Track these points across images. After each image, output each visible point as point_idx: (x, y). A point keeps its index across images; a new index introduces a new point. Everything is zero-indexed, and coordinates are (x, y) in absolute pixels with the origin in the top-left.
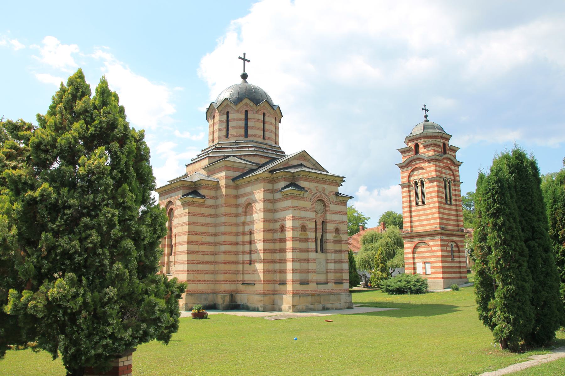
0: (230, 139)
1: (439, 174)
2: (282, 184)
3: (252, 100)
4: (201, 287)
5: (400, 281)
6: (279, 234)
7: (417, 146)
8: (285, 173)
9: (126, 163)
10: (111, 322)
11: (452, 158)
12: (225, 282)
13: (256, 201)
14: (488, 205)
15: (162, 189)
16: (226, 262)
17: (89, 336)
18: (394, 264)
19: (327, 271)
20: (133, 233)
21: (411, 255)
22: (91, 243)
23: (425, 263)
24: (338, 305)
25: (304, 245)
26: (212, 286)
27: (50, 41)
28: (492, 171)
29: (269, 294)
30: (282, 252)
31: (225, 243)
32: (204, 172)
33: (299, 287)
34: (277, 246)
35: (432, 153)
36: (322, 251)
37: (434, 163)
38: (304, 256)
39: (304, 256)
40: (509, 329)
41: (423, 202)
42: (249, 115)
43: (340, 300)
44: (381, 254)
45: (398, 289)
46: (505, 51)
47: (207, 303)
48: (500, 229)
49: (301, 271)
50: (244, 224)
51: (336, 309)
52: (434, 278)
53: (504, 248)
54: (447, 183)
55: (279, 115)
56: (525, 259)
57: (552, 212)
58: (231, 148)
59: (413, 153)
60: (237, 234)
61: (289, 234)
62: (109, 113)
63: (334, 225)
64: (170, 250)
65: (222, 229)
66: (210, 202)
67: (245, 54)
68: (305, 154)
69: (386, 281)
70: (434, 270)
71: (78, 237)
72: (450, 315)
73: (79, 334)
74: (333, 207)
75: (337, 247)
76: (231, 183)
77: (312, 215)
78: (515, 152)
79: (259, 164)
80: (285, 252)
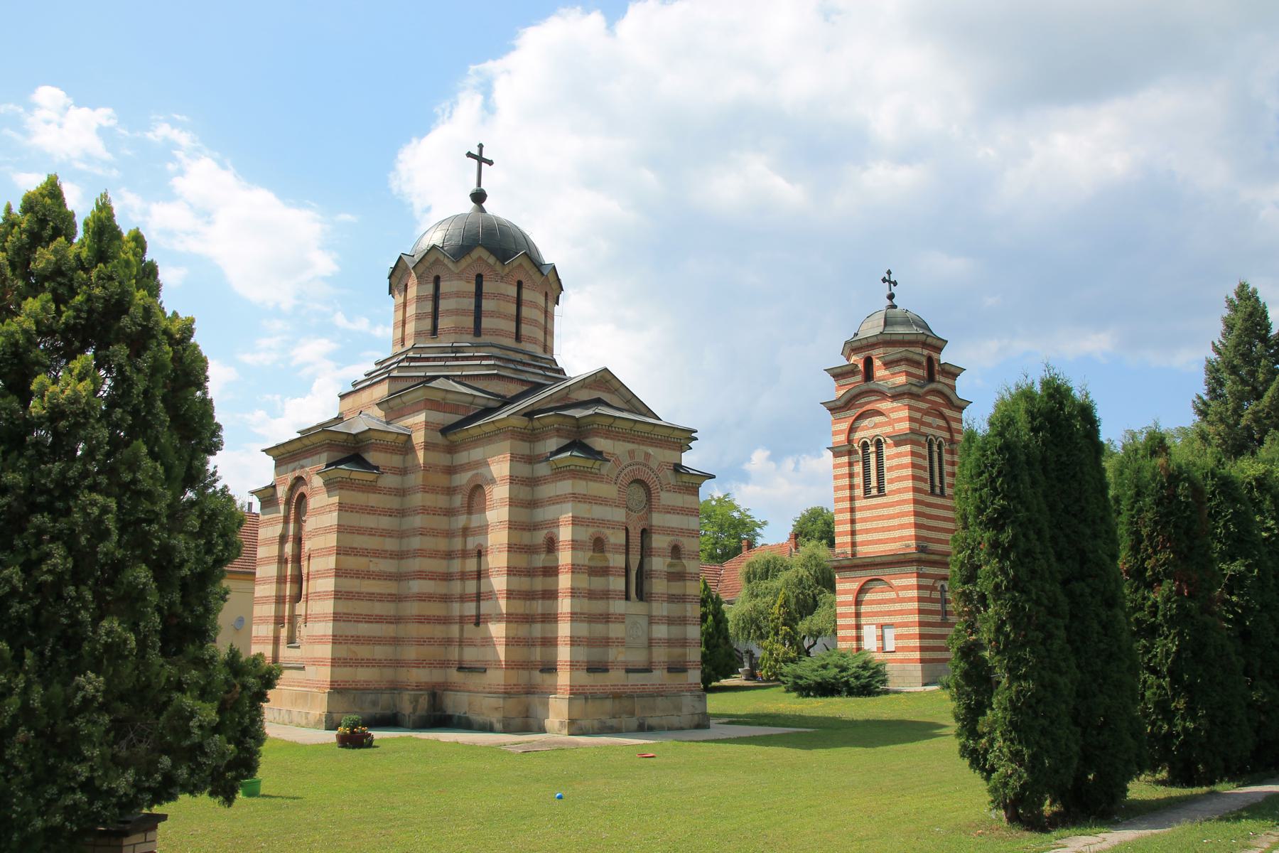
0: (441, 337)
1: (916, 426)
2: (552, 444)
3: (493, 251)
4: (364, 675)
5: (824, 667)
6: (543, 556)
7: (868, 362)
8: (561, 419)
9: (146, 392)
10: (88, 754)
11: (947, 390)
12: (419, 664)
13: (493, 481)
14: (982, 502)
15: (282, 450)
16: (423, 620)
17: (33, 787)
18: (814, 628)
19: (651, 643)
20: (154, 553)
21: (852, 609)
22: (49, 572)
23: (882, 626)
24: (675, 721)
25: (598, 583)
26: (389, 673)
27: (48, 95)
28: (991, 424)
29: (518, 693)
30: (549, 598)
31: (421, 575)
32: (379, 413)
33: (584, 678)
34: (539, 584)
35: (901, 379)
36: (642, 595)
37: (906, 401)
38: (598, 607)
39: (598, 607)
40: (1020, 777)
41: (880, 489)
42: (442, 284)
43: (678, 708)
44: (786, 603)
45: (819, 684)
46: (1083, 152)
47: (378, 711)
48: (1004, 557)
49: (591, 642)
50: (466, 531)
51: (670, 729)
52: (902, 661)
53: (1013, 598)
54: (935, 448)
55: (555, 286)
56: (1061, 622)
57: (1133, 517)
58: (441, 359)
59: (859, 378)
60: (449, 555)
61: (565, 557)
62: (111, 278)
63: (669, 539)
64: (296, 590)
65: (416, 543)
66: (389, 481)
67: (481, 146)
68: (609, 377)
69: (794, 666)
70: (901, 643)
71: (21, 559)
72: (922, 745)
73: (8, 781)
74: (667, 498)
75: (676, 588)
76: (439, 438)
77: (619, 515)
78: (1047, 384)
79: (503, 397)
80: (557, 598)
